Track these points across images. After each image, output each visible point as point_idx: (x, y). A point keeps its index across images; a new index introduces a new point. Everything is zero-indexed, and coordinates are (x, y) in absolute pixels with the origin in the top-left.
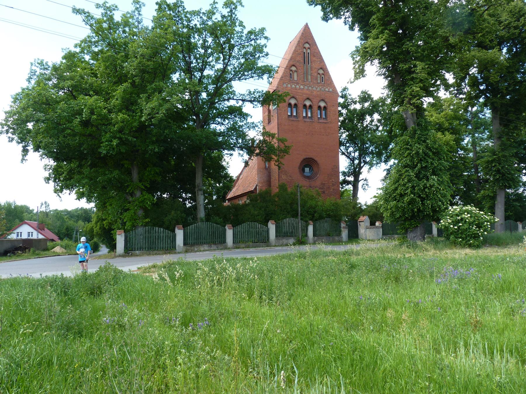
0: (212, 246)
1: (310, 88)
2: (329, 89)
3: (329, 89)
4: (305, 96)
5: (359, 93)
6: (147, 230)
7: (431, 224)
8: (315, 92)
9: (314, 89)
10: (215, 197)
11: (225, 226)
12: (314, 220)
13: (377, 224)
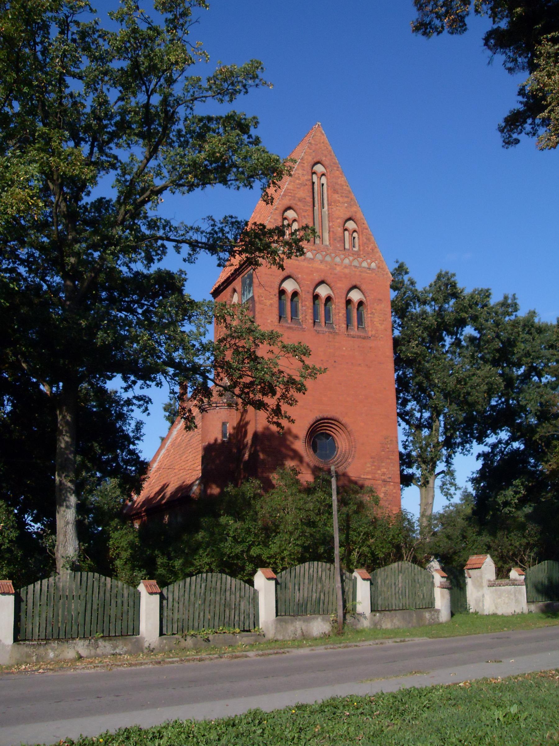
0: (101, 643)
1: (328, 259)
2: (369, 264)
3: (369, 264)
4: (317, 278)
5: (432, 279)
6: (45, 588)
7: (137, 597)
8: (338, 269)
9: (338, 260)
10: (475, 413)
11: (135, 586)
12: (373, 564)
13: (514, 574)
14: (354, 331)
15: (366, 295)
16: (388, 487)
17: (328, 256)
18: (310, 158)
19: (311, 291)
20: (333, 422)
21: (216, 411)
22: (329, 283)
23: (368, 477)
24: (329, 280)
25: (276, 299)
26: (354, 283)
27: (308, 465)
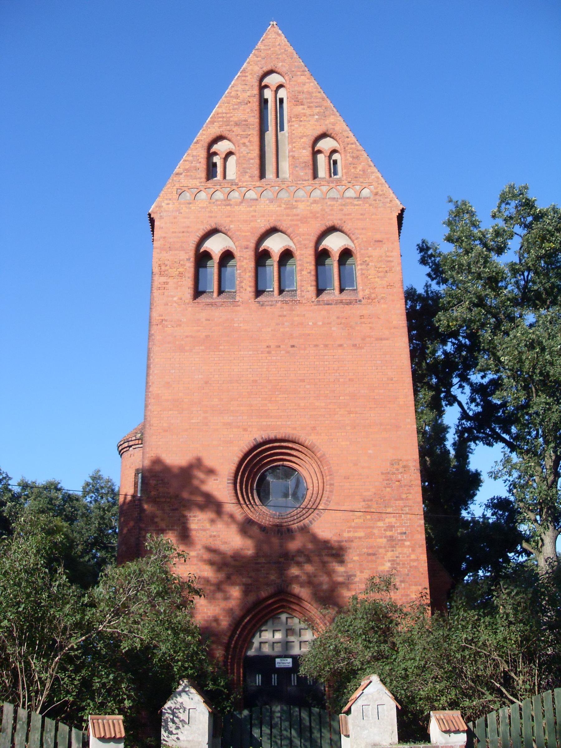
8: (301, 206)
14: (333, 294)
15: (353, 237)
16: (399, 550)
17: (283, 191)
18: (256, 68)
19: (252, 245)
20: (290, 445)
21: (129, 453)
22: (284, 229)
23: (357, 535)
24: (283, 226)
25: (190, 266)
26: (329, 224)
27: (232, 516)
